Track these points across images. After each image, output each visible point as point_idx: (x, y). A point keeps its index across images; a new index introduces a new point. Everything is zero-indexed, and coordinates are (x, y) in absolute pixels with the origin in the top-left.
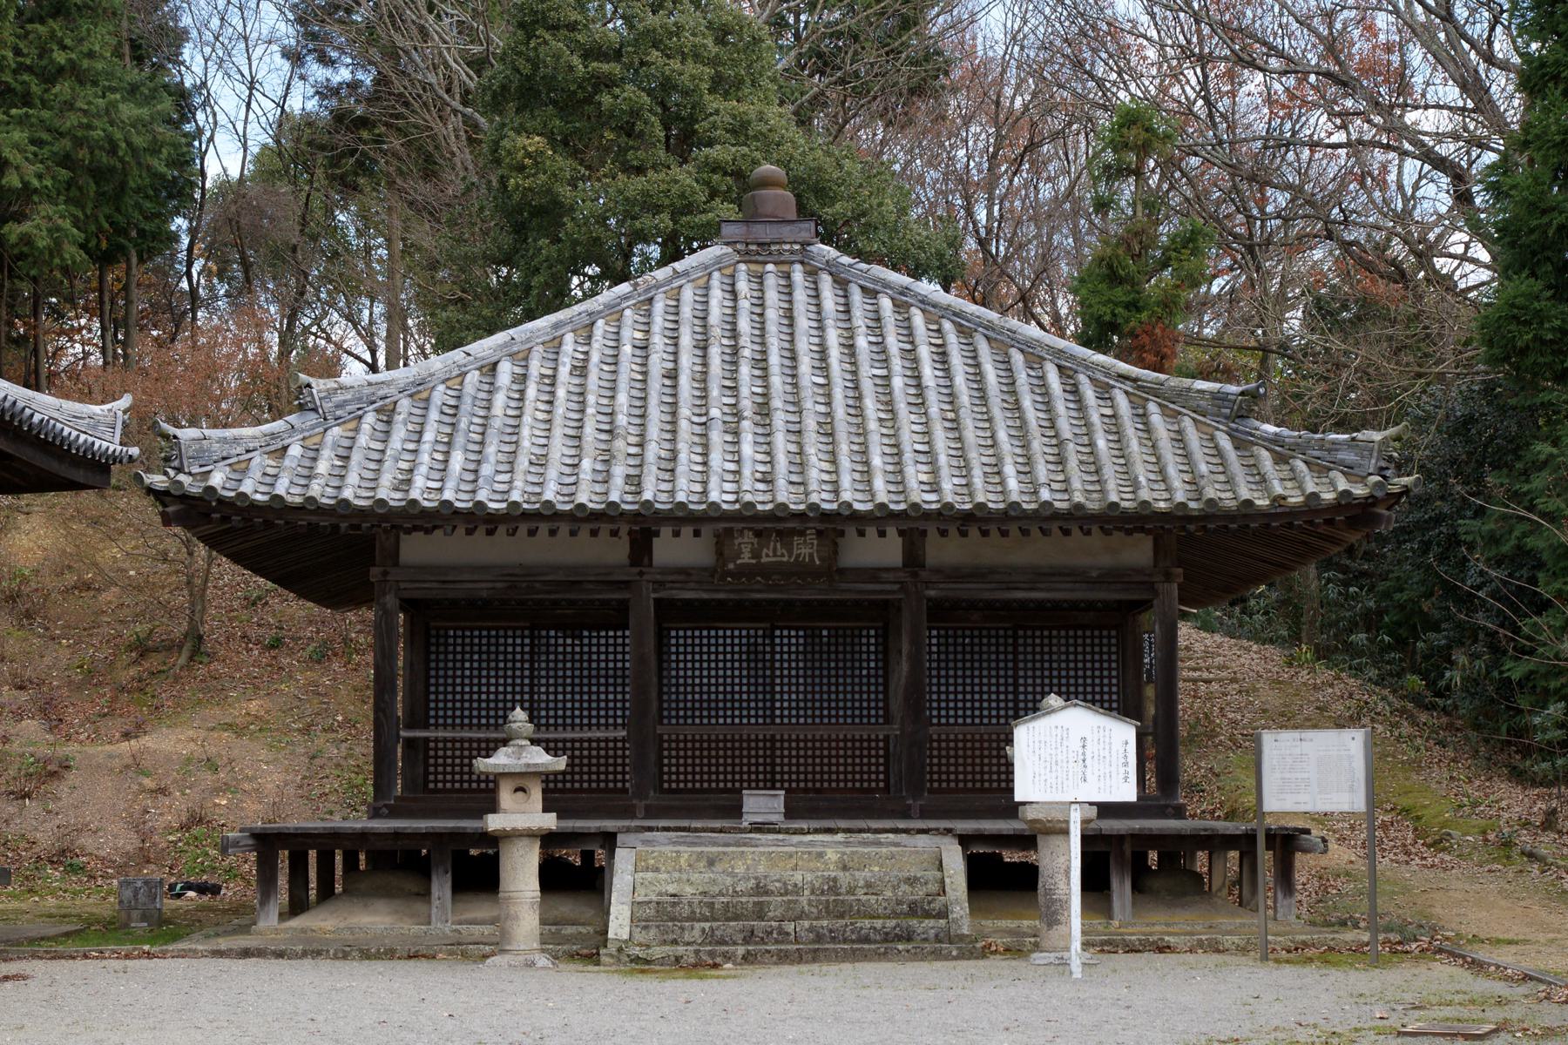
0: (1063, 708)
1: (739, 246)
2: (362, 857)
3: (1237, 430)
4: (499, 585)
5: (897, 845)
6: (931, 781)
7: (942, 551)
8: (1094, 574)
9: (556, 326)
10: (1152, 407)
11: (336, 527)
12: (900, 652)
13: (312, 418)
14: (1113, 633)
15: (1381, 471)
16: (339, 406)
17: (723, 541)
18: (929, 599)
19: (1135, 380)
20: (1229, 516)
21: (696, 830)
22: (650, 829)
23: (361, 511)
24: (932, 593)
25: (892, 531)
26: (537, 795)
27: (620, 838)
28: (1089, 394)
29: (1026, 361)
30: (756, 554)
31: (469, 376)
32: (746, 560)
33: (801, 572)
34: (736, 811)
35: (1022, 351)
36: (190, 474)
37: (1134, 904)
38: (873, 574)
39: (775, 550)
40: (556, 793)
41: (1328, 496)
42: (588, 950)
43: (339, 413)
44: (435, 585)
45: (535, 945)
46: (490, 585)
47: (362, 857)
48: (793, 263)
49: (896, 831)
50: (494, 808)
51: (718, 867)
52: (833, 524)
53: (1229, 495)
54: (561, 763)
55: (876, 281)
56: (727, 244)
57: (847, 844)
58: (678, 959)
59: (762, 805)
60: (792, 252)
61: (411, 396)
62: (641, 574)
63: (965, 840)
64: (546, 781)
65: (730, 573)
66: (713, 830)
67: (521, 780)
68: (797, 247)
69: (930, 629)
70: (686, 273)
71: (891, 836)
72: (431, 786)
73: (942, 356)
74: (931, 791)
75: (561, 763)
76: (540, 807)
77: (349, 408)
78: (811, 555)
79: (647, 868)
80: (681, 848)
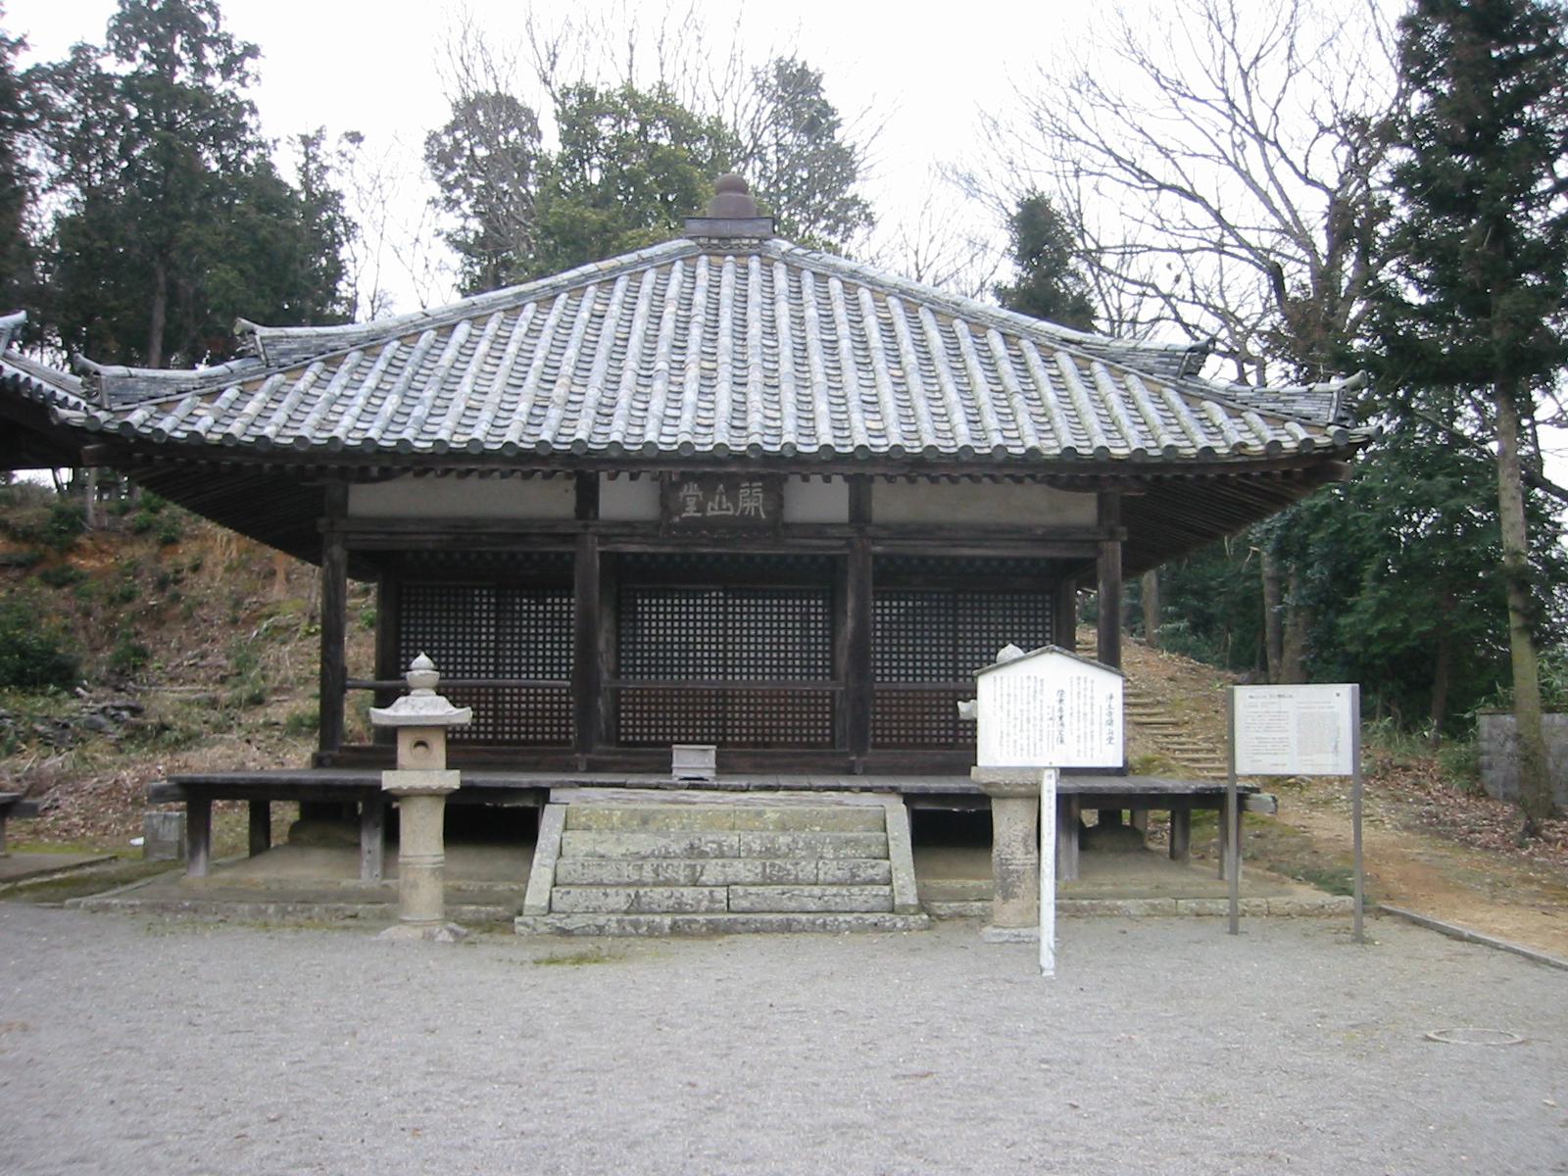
0: (1020, 659)
1: (701, 241)
2: (360, 805)
3: (1185, 386)
4: (445, 537)
5: (840, 803)
6: (875, 736)
7: (892, 504)
8: (1040, 532)
9: (519, 296)
10: (1097, 367)
11: (259, 467)
12: (846, 612)
13: (253, 365)
14: (1047, 597)
15: (1339, 420)
16: (283, 354)
17: (668, 492)
18: (877, 557)
19: (1079, 343)
20: (1187, 464)
21: (631, 787)
22: (584, 785)
23: (285, 450)
24: (878, 549)
25: (837, 480)
26: (439, 749)
27: (553, 794)
28: (1034, 357)
29: (970, 331)
30: (701, 508)
31: (425, 335)
32: (692, 514)
33: (745, 526)
34: (666, 768)
35: (967, 322)
36: (109, 410)
37: (1080, 856)
38: (819, 529)
39: (720, 503)
40: (460, 747)
41: (1289, 445)
42: (491, 919)
43: (283, 361)
44: (383, 537)
45: (438, 916)
46: (435, 537)
47: (360, 805)
48: (750, 255)
49: (838, 789)
50: (392, 764)
51: (652, 827)
52: (776, 469)
53: (1187, 443)
54: (463, 715)
55: (827, 266)
56: (691, 238)
57: (788, 802)
58: (601, 928)
59: (693, 760)
60: (751, 246)
61: (362, 350)
62: (586, 527)
63: (909, 798)
64: (447, 732)
65: (675, 526)
66: (649, 787)
67: (422, 732)
68: (755, 242)
69: (875, 600)
70: (650, 260)
71: (833, 793)
72: (623, 738)
73: (888, 327)
74: (875, 746)
75: (463, 715)
76: (443, 764)
77: (295, 357)
78: (757, 509)
79: (588, 827)
80: (614, 804)
